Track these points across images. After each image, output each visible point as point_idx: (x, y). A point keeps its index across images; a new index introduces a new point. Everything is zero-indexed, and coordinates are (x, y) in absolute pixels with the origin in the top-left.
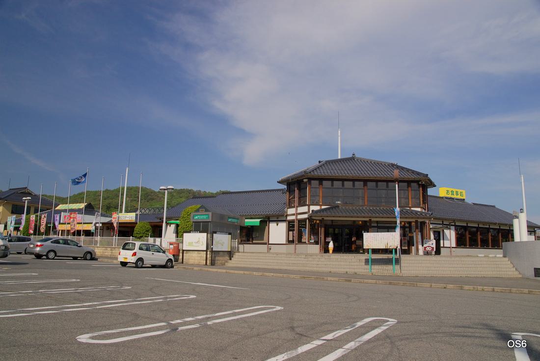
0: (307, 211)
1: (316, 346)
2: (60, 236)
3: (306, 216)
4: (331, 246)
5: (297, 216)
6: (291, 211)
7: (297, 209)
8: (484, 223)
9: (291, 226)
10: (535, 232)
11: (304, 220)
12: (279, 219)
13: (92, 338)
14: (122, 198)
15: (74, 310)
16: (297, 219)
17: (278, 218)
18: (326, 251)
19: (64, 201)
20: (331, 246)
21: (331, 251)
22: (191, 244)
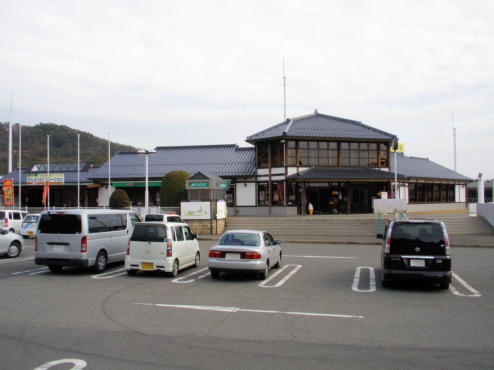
0: (284, 172)
1: (272, 278)
2: (45, 207)
3: (283, 178)
4: (158, 200)
5: (270, 178)
6: (261, 172)
7: (270, 171)
8: (430, 179)
9: (260, 188)
10: (466, 184)
11: (281, 182)
12: (247, 180)
13: (178, 281)
14: (15, 157)
15: (6, 262)
16: (271, 181)
17: (246, 179)
18: (308, 213)
19: (444, 193)
20: (311, 207)
21: (311, 213)
22: (190, 213)
